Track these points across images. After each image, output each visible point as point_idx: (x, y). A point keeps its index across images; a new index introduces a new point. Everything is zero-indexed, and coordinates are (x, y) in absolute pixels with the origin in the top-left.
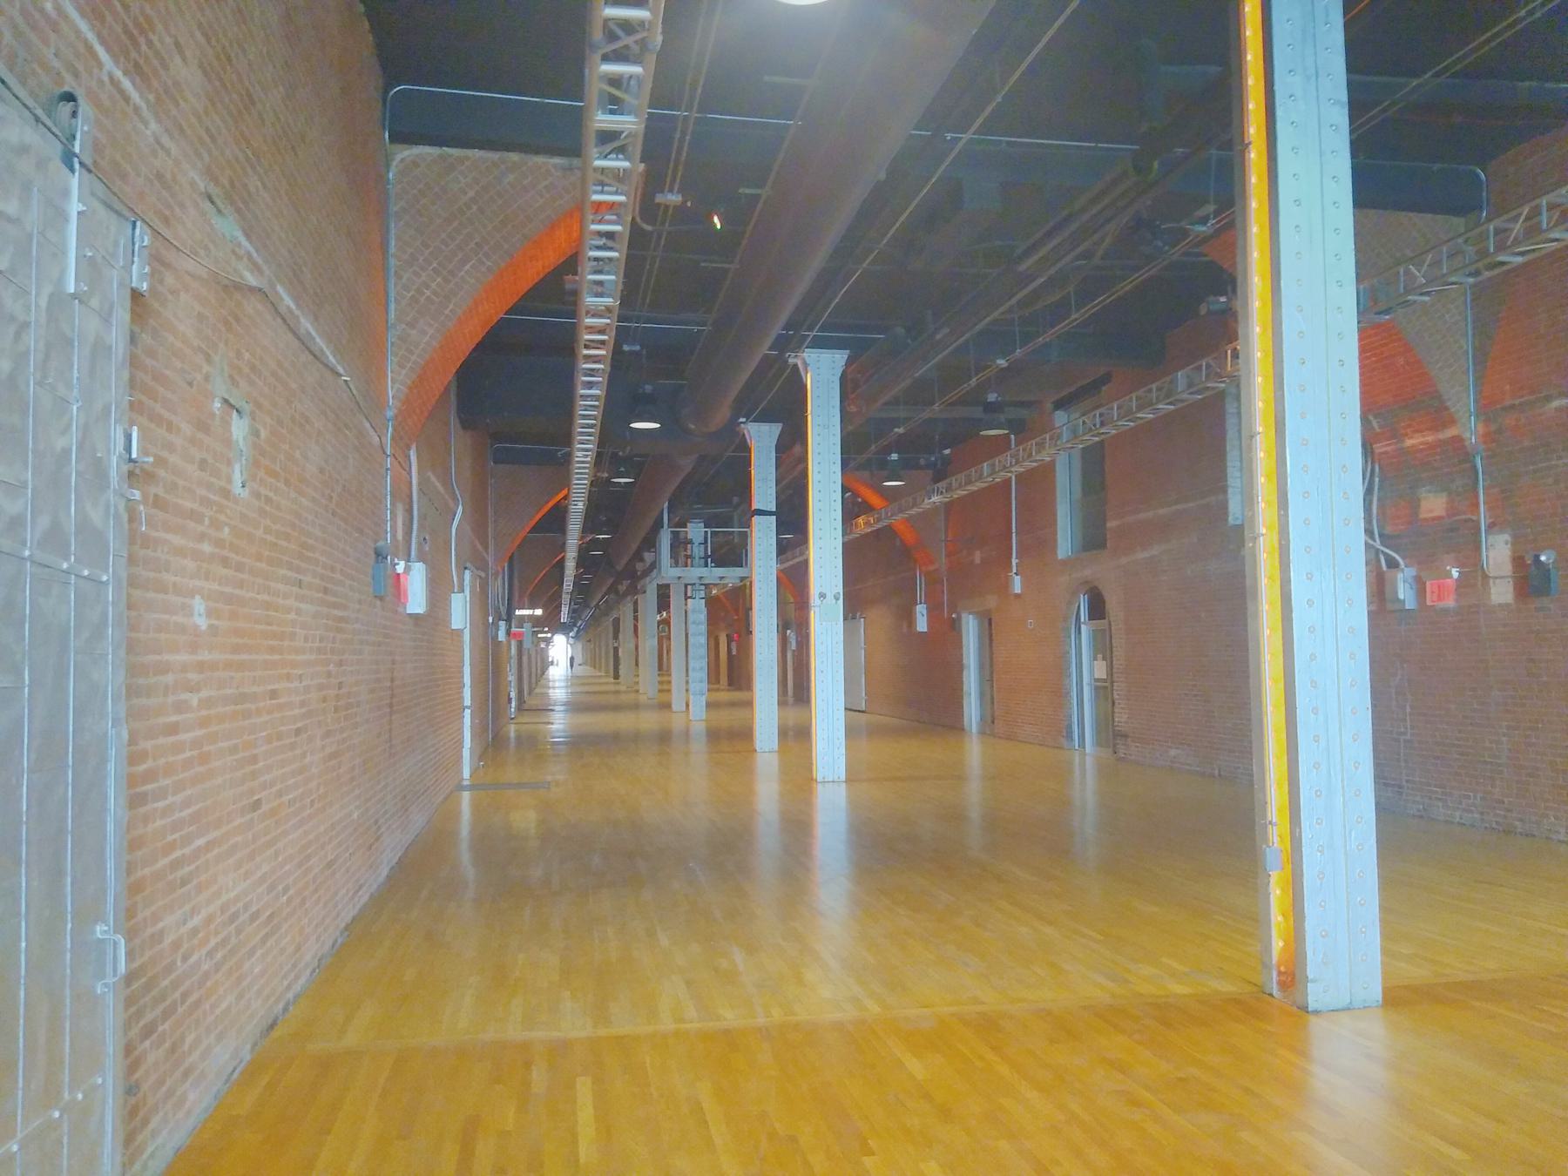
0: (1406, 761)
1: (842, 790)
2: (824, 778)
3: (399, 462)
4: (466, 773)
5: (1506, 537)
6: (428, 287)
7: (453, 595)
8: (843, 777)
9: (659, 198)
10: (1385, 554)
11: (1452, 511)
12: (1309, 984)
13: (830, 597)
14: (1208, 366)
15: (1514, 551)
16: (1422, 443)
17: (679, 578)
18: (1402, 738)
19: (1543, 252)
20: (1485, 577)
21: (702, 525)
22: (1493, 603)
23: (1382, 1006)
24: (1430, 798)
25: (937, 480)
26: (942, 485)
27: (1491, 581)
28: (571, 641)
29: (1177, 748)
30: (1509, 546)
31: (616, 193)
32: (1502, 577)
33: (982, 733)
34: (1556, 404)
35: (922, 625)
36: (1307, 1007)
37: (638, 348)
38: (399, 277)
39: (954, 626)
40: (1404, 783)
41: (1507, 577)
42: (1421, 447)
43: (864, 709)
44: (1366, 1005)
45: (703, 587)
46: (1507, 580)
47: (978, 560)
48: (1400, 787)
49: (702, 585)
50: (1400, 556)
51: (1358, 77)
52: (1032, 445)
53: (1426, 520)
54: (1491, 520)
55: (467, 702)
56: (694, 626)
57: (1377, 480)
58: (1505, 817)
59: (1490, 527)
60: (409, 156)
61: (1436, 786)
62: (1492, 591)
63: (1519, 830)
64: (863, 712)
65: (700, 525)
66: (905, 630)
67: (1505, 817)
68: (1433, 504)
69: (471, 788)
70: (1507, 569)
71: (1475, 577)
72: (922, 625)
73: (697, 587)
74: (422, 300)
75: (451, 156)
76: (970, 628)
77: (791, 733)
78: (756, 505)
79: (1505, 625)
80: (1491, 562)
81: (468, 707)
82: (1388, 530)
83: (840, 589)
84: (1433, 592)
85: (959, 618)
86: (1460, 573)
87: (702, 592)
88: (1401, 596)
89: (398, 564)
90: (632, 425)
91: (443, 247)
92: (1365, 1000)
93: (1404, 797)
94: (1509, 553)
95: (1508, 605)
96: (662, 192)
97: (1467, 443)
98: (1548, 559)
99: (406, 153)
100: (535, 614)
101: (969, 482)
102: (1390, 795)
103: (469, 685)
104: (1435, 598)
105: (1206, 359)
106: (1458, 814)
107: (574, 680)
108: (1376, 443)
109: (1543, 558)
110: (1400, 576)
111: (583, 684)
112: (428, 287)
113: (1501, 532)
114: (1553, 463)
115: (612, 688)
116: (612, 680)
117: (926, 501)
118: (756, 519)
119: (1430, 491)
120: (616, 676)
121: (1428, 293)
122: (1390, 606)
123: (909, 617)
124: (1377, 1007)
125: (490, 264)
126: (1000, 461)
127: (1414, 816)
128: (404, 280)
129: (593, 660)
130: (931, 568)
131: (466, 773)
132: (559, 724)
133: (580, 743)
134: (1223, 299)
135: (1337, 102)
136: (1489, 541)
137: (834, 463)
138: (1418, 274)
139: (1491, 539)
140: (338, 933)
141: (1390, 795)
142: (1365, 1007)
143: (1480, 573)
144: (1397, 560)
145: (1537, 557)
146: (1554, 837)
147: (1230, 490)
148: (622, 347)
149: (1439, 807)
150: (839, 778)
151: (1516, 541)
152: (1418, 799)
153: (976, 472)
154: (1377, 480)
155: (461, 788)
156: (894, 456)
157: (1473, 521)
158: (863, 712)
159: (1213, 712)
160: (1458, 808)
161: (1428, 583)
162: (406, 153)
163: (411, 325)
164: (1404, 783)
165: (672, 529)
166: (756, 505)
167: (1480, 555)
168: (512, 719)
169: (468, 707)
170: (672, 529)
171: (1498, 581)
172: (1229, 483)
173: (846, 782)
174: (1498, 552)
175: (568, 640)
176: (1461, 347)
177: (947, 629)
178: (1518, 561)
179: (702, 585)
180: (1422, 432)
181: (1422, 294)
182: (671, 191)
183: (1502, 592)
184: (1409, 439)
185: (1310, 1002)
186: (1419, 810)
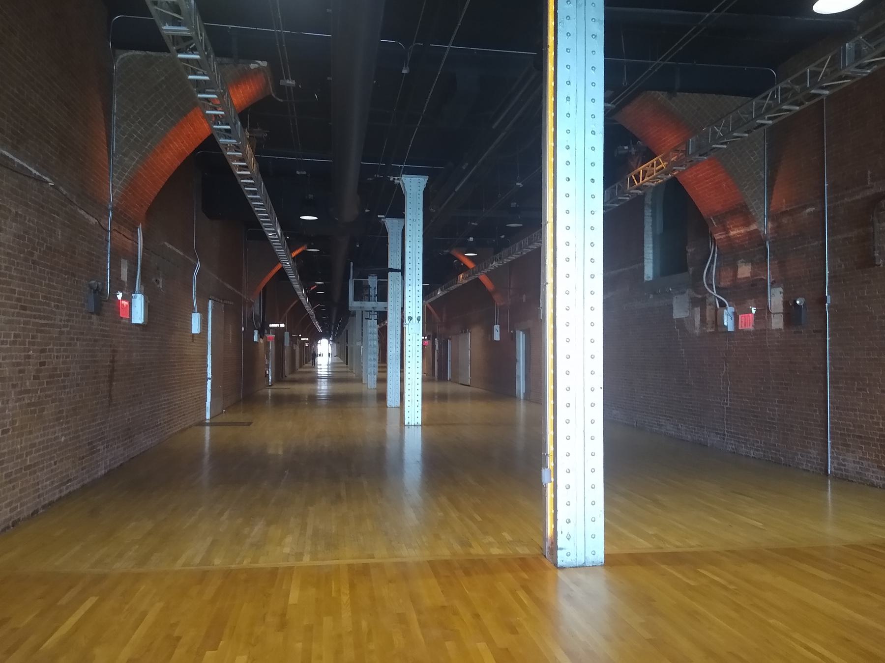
0: (727, 420)
1: (419, 431)
2: (409, 423)
3: (123, 235)
4: (208, 416)
5: (781, 289)
6: (136, 133)
7: (193, 314)
8: (420, 423)
9: (282, 82)
10: (718, 298)
11: (753, 274)
12: (558, 551)
13: (415, 319)
14: (619, 186)
15: (784, 298)
16: (738, 234)
17: (361, 307)
18: (725, 406)
19: (783, 117)
20: (769, 313)
21: (376, 277)
22: (772, 328)
23: (604, 565)
24: (739, 442)
25: (495, 253)
26: (498, 256)
27: (772, 315)
28: (331, 343)
29: (617, 410)
30: (782, 294)
31: (204, 75)
32: (777, 313)
33: (525, 399)
34: (808, 210)
35: (497, 337)
36: (557, 565)
37: (305, 173)
38: (118, 127)
39: (513, 339)
40: (726, 433)
41: (781, 313)
42: (738, 236)
43: (469, 384)
44: (594, 565)
45: (376, 313)
46: (780, 315)
47: (524, 300)
48: (724, 435)
49: (375, 311)
50: (727, 301)
51: (608, 8)
52: (538, 233)
53: (740, 279)
54: (773, 279)
55: (209, 376)
56: (371, 335)
57: (716, 255)
58: (776, 454)
59: (772, 284)
60: (126, 56)
61: (742, 435)
62: (773, 321)
63: (783, 462)
64: (469, 386)
65: (375, 277)
66: (489, 339)
67: (776, 454)
68: (745, 271)
69: (210, 424)
70: (781, 309)
71: (764, 312)
72: (497, 337)
73: (373, 313)
74: (132, 140)
75: (152, 55)
76: (521, 338)
77: (436, 397)
78: (390, 266)
79: (778, 342)
80: (772, 304)
81: (210, 379)
82: (722, 284)
83: (421, 315)
84: (742, 322)
85: (515, 333)
86: (756, 310)
87: (376, 316)
88: (726, 324)
89: (118, 294)
90: (301, 217)
91: (145, 109)
92: (593, 562)
93: (725, 441)
94: (782, 299)
95: (780, 329)
96: (283, 79)
97: (762, 234)
98: (800, 303)
99: (125, 55)
100: (281, 326)
101: (510, 255)
102: (719, 439)
103: (211, 366)
104: (743, 326)
105: (618, 183)
106: (752, 452)
107: (333, 365)
108: (716, 234)
109: (798, 302)
110: (725, 311)
111: (338, 367)
112: (136, 133)
113: (778, 286)
114: (806, 246)
115: (345, 369)
116: (345, 365)
117: (490, 265)
118: (390, 274)
119: (743, 262)
120: (347, 364)
121: (725, 143)
122: (719, 329)
123: (491, 332)
124: (601, 566)
125: (172, 119)
126: (524, 242)
127: (730, 452)
128: (122, 129)
129: (339, 354)
130: (3, 298)
131: (208, 416)
132: (323, 388)
133: (336, 399)
134: (626, 148)
135: (599, 20)
136: (772, 292)
137: (419, 242)
138: (718, 130)
139: (773, 290)
140: (40, 507)
141: (719, 439)
142: (593, 566)
143: (766, 310)
144: (725, 302)
145: (795, 302)
146: (801, 467)
147: (646, 261)
148: (296, 172)
149: (742, 447)
150: (409, 423)
151: (785, 293)
152: (732, 442)
153: (513, 248)
154: (716, 255)
155: (202, 424)
156: (471, 239)
157: (764, 279)
158: (469, 386)
159: (634, 389)
160: (752, 448)
161: (740, 316)
162: (124, 55)
163: (125, 155)
164: (726, 433)
165: (355, 279)
166: (390, 266)
167: (767, 301)
168: (270, 386)
169: (210, 379)
170: (355, 279)
171: (775, 315)
172: (645, 256)
173: (421, 425)
174: (776, 299)
175: (329, 343)
176: (760, 177)
177: (510, 340)
178: (786, 304)
179: (375, 311)
180: (738, 227)
181: (722, 144)
182: (287, 78)
183: (777, 322)
184: (732, 231)
185: (558, 561)
186: (733, 449)
